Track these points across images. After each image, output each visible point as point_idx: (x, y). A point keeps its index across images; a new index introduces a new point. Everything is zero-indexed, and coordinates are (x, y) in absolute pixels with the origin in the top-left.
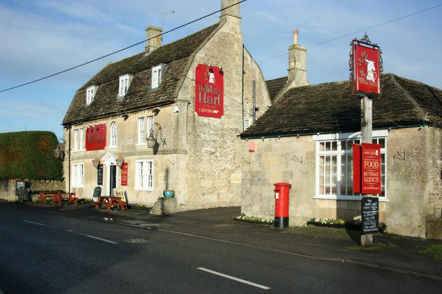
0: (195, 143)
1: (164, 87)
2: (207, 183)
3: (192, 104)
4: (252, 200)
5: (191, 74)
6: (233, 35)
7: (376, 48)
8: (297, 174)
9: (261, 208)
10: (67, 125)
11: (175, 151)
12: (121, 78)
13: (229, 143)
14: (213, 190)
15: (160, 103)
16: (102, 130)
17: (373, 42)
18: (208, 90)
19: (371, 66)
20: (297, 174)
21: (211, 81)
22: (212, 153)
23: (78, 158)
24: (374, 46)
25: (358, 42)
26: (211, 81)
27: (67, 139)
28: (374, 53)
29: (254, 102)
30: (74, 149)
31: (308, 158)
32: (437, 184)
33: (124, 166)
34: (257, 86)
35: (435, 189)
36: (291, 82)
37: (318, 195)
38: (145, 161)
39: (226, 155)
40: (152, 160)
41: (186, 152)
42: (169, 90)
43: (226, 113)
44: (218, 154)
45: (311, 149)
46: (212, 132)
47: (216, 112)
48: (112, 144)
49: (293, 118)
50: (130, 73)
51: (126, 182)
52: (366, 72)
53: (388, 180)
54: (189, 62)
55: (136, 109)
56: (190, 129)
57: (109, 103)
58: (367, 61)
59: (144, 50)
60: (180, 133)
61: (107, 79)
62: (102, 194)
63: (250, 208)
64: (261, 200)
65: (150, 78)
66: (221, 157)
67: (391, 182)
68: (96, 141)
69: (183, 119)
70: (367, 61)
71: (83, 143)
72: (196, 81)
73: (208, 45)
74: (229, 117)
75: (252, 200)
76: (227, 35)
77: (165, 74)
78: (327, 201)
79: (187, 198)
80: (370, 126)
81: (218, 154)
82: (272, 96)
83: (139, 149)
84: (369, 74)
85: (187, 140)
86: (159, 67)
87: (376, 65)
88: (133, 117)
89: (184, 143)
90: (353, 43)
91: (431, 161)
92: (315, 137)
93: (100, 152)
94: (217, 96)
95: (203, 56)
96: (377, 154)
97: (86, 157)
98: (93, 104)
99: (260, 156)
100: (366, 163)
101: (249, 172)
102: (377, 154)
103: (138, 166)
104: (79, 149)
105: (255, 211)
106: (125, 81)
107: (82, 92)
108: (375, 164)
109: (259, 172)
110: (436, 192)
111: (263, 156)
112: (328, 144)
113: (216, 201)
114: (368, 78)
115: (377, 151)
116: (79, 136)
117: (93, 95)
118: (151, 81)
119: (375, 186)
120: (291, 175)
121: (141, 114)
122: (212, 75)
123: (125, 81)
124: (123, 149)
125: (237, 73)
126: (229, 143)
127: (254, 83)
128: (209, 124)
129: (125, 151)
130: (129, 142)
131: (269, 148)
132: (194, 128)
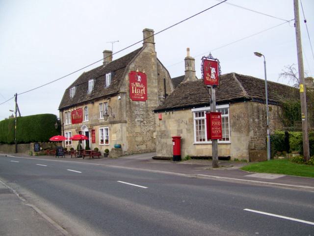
0: (131, 116)
1: (112, 86)
2: (139, 139)
3: (128, 94)
4: (162, 147)
5: (127, 78)
6: (151, 54)
7: (216, 61)
8: (184, 131)
9: (167, 151)
10: (61, 109)
11: (120, 122)
12: (107, 75)
13: (151, 115)
14: (143, 142)
15: (111, 94)
16: (80, 112)
17: (215, 57)
18: (137, 86)
19: (213, 70)
20: (184, 131)
21: (139, 80)
22: (142, 122)
23: (68, 129)
24: (215, 59)
25: (206, 58)
26: (139, 80)
27: (61, 118)
28: (215, 64)
29: (165, 91)
30: (66, 123)
31: (189, 122)
32: (256, 133)
33: (93, 131)
34: (167, 81)
35: (255, 135)
36: (187, 78)
37: (196, 142)
38: (104, 128)
39: (150, 122)
40: (108, 128)
41: (126, 122)
42: (115, 87)
43: (149, 98)
44: (145, 122)
45: (191, 117)
46: (141, 109)
47: (142, 98)
48: (86, 120)
49: (182, 99)
50: (93, 78)
51: (95, 140)
52: (210, 74)
53: (230, 132)
54: (126, 70)
55: (97, 99)
56: (128, 109)
57: (83, 96)
58: (211, 68)
59: (102, 64)
60: (123, 111)
61: (81, 83)
62: (37, 145)
63: (161, 152)
64: (166, 147)
65: (105, 80)
66: (147, 123)
67: (232, 133)
68: (76, 120)
69: (124, 103)
70: (211, 68)
71: (70, 120)
72: (17, 118)
73: (137, 60)
74: (151, 100)
75: (162, 147)
76: (147, 54)
77: (113, 77)
78: (225, 145)
79: (128, 148)
80: (215, 103)
81: (145, 122)
82: (175, 87)
83: (100, 121)
84: (212, 75)
85: (127, 115)
86: (110, 74)
87: (216, 70)
88: (97, 104)
89: (125, 117)
90: (203, 57)
91: (252, 120)
92: (193, 110)
93: (80, 124)
94: (143, 89)
95: (134, 66)
96: (219, 118)
97: (72, 128)
98: (75, 96)
99: (165, 122)
100: (213, 123)
101: (160, 131)
102: (219, 118)
103: (100, 132)
104: (68, 123)
105: (164, 153)
106: (91, 83)
107: (68, 91)
108: (219, 123)
109: (164, 131)
110: (255, 137)
111: (166, 122)
112: (200, 113)
113: (145, 149)
114: (211, 77)
115: (219, 116)
116: (68, 117)
117: (75, 92)
118: (105, 82)
119: (219, 135)
120: (181, 131)
121: (100, 102)
122: (139, 77)
123: (91, 83)
124: (92, 122)
125: (154, 75)
126: (151, 115)
127: (165, 79)
128: (139, 105)
129: (93, 123)
130: (95, 118)
131: (169, 118)
132: (130, 108)
